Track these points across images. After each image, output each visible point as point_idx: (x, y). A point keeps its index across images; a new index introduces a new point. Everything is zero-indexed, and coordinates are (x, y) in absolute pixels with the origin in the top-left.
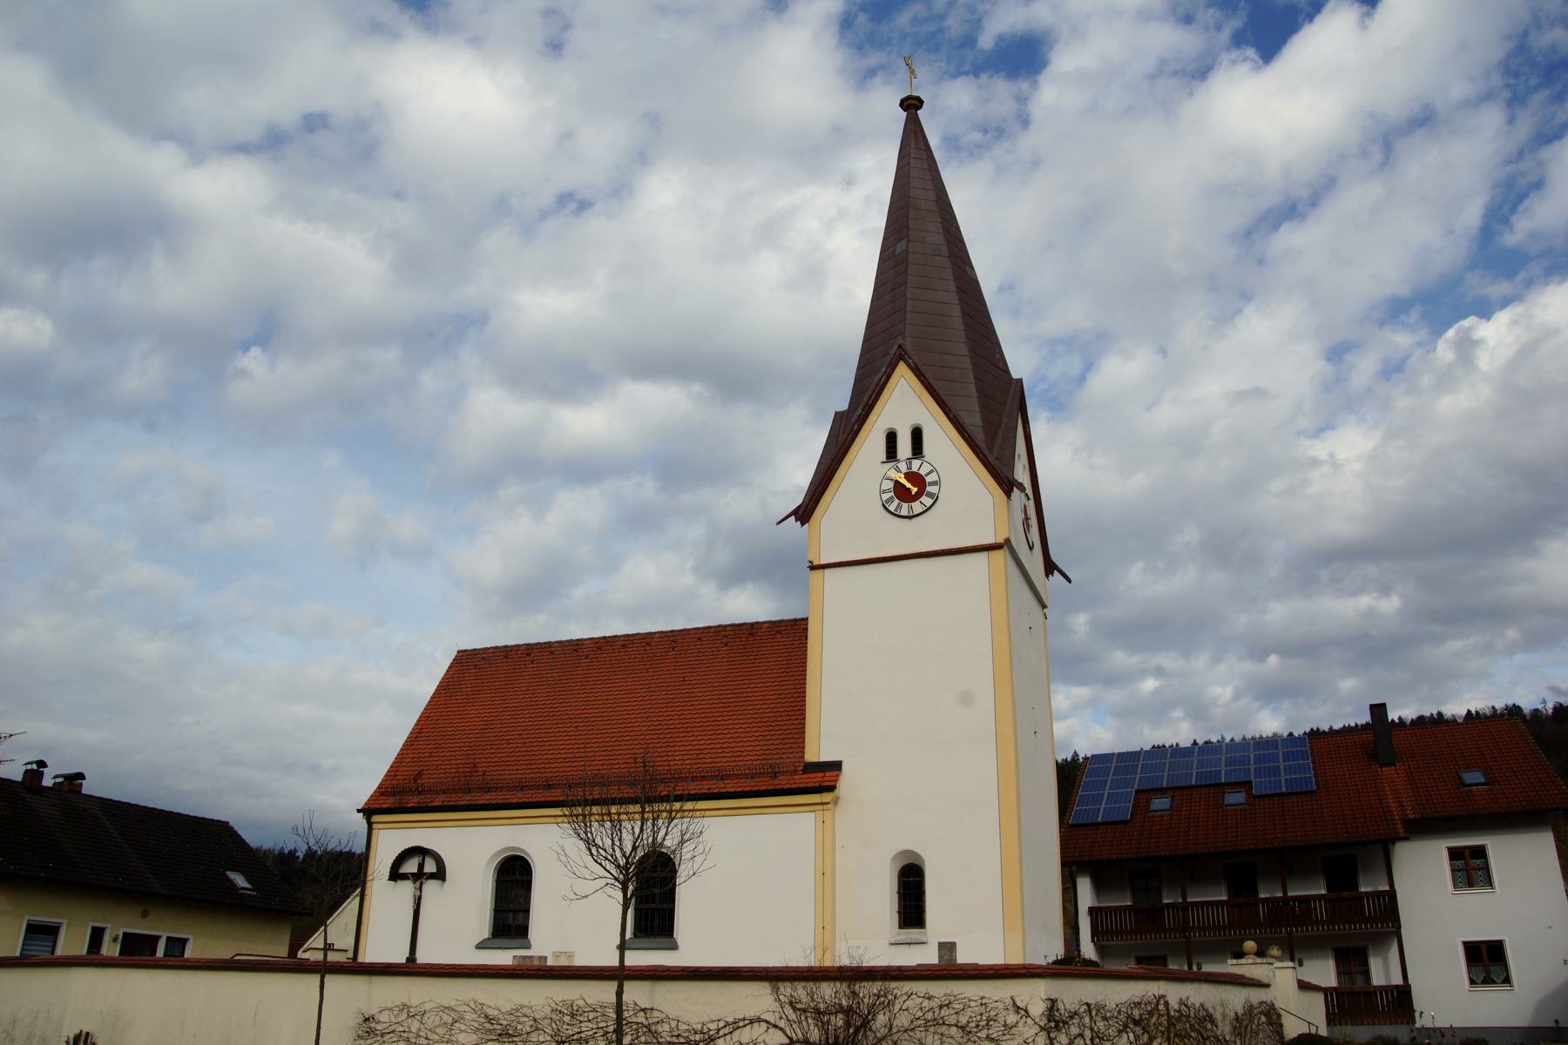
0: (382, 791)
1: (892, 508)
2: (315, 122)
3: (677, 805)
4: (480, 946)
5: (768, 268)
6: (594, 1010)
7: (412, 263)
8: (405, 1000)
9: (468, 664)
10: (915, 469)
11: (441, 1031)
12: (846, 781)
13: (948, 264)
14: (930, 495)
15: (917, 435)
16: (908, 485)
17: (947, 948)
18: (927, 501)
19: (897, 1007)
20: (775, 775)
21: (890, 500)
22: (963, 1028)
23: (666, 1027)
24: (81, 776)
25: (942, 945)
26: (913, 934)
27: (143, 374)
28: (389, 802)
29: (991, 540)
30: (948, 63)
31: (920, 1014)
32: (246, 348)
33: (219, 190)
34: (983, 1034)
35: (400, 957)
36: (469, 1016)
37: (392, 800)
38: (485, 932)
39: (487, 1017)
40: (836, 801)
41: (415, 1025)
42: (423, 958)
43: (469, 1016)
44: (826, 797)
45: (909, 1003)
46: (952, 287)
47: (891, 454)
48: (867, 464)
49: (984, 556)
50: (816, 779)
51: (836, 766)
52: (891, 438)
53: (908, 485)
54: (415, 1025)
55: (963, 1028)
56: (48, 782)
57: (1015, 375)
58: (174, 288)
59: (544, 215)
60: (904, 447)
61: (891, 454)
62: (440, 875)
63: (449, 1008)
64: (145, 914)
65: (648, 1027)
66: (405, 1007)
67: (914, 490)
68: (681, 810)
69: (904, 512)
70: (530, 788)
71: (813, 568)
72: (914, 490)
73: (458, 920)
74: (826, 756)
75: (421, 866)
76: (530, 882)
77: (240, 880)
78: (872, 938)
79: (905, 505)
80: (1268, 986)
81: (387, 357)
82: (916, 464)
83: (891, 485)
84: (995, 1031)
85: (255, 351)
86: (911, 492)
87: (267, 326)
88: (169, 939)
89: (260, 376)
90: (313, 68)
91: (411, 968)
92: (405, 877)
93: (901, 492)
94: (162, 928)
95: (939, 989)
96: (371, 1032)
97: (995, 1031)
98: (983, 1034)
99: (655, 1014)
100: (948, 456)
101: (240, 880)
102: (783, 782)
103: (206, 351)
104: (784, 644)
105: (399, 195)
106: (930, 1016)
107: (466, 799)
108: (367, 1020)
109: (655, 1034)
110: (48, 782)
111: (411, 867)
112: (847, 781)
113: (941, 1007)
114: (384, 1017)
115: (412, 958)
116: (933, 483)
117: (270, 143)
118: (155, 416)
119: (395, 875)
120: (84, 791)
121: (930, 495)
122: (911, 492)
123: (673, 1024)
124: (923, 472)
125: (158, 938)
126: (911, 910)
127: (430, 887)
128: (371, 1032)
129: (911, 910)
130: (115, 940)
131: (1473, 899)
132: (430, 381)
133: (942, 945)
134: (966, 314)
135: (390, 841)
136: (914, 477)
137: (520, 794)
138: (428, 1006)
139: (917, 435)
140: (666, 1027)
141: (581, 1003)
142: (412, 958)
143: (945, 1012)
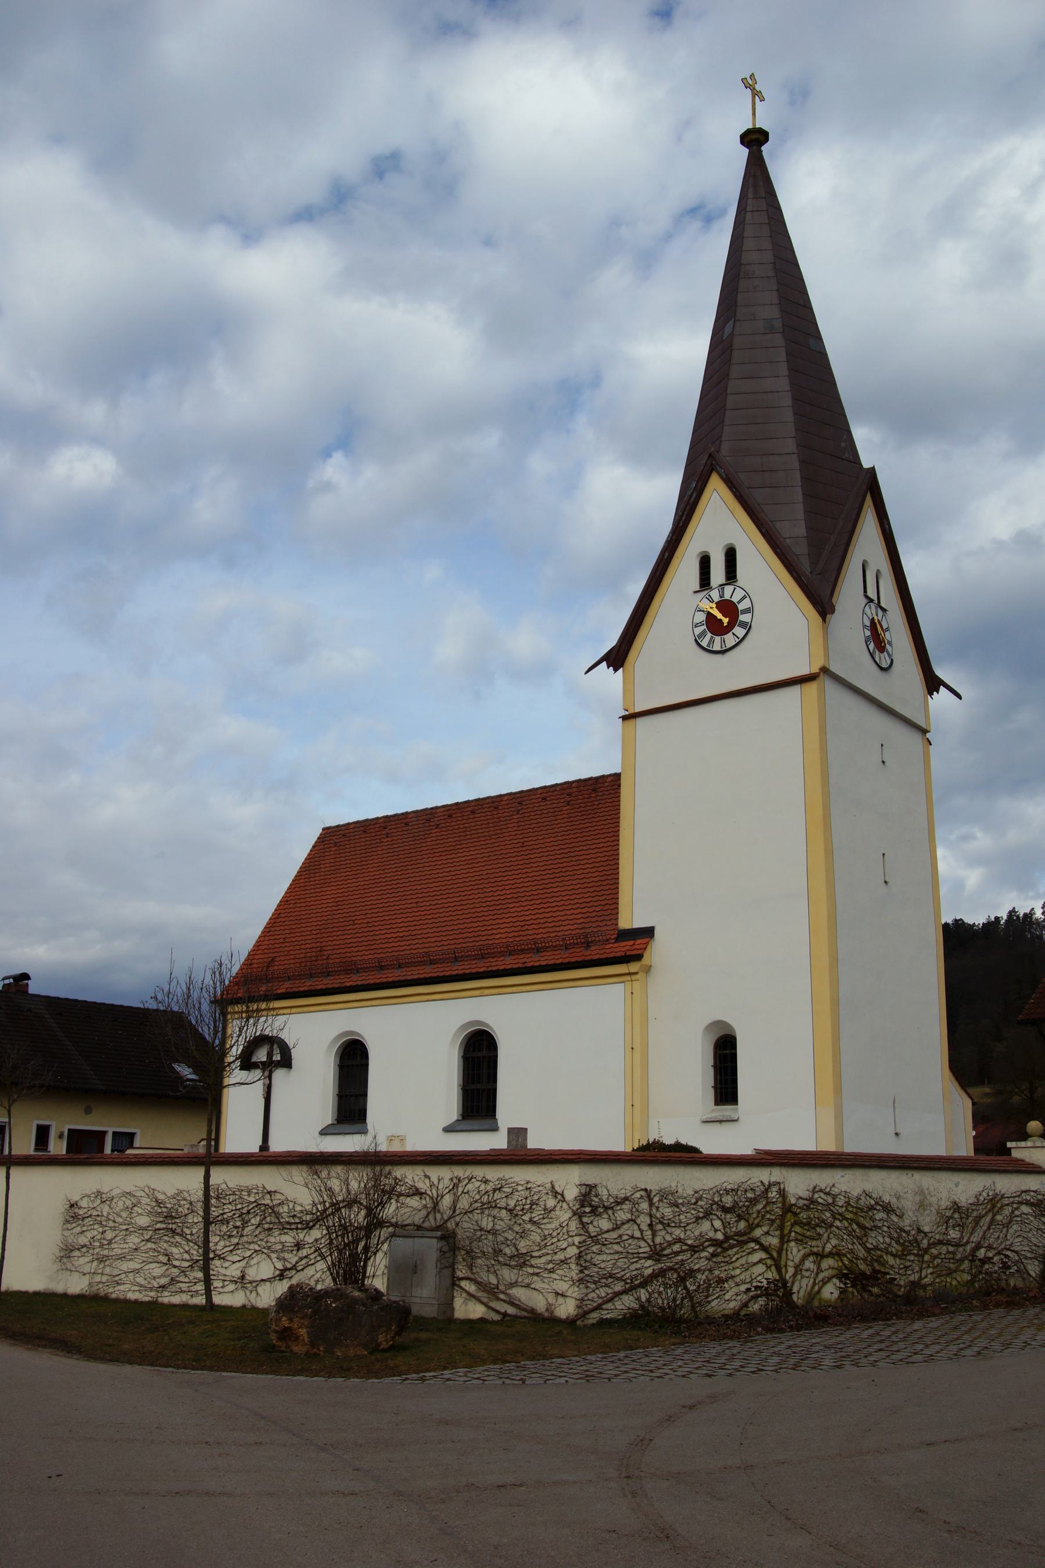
1: (704, 643)
2: (385, 165)
3: (263, 1006)
4: (324, 1133)
5: (951, 263)
6: (234, 1194)
7: (506, 324)
8: (99, 1188)
9: (335, 842)
10: (727, 597)
11: (124, 1214)
13: (778, 340)
14: (743, 625)
15: (731, 555)
16: (719, 616)
17: (518, 1134)
18: (739, 631)
19: (460, 1189)
20: (588, 945)
21: (702, 635)
22: (511, 1211)
23: (286, 1208)
25: (511, 1131)
26: (726, 1110)
27: (214, 502)
29: (804, 671)
31: (477, 1197)
32: (327, 454)
33: (281, 272)
34: (526, 1218)
36: (145, 1200)
38: (328, 1116)
39: (157, 1201)
40: (648, 969)
41: (106, 1209)
43: (145, 1200)
44: (634, 967)
45: (470, 1187)
46: (783, 369)
48: (682, 602)
49: (796, 690)
51: (648, 933)
52: (705, 562)
53: (719, 616)
54: (106, 1209)
55: (511, 1211)
57: (866, 464)
58: (256, 389)
59: (668, 237)
62: (286, 1062)
63: (129, 1193)
64: (88, 1111)
65: (272, 1208)
66: (99, 1193)
67: (726, 621)
68: (269, 1009)
69: (717, 647)
70: (408, 965)
72: (726, 621)
73: (301, 1108)
74: (638, 923)
75: (270, 1055)
76: (367, 1065)
77: (185, 1071)
78: (681, 1112)
79: (718, 639)
81: (489, 442)
82: (728, 590)
83: (701, 617)
84: (537, 1214)
85: (338, 457)
86: (724, 622)
87: (348, 425)
88: (114, 1133)
89: (347, 486)
90: (373, 97)
91: (264, 1158)
93: (714, 626)
94: (107, 1122)
95: (493, 1173)
96: (75, 1217)
97: (537, 1214)
98: (526, 1218)
99: (278, 1196)
101: (185, 1071)
102: (594, 953)
103: (281, 461)
105: (488, 242)
106: (485, 1199)
107: (308, 985)
108: (72, 1206)
109: (278, 1215)
111: (261, 1055)
112: (658, 951)
113: (494, 1190)
114: (84, 1203)
115: (265, 1146)
116: (746, 611)
117: (332, 206)
118: (234, 550)
119: (247, 1063)
121: (743, 625)
122: (724, 622)
123: (291, 1205)
124: (735, 599)
125: (104, 1133)
126: (726, 1088)
127: (279, 1074)
128: (75, 1217)
129: (726, 1088)
130: (61, 1136)
132: (540, 465)
133: (511, 1131)
134: (800, 400)
136: (728, 607)
137: (398, 972)
138: (115, 1193)
139: (731, 555)
140: (286, 1208)
141: (224, 1186)
143: (497, 1195)
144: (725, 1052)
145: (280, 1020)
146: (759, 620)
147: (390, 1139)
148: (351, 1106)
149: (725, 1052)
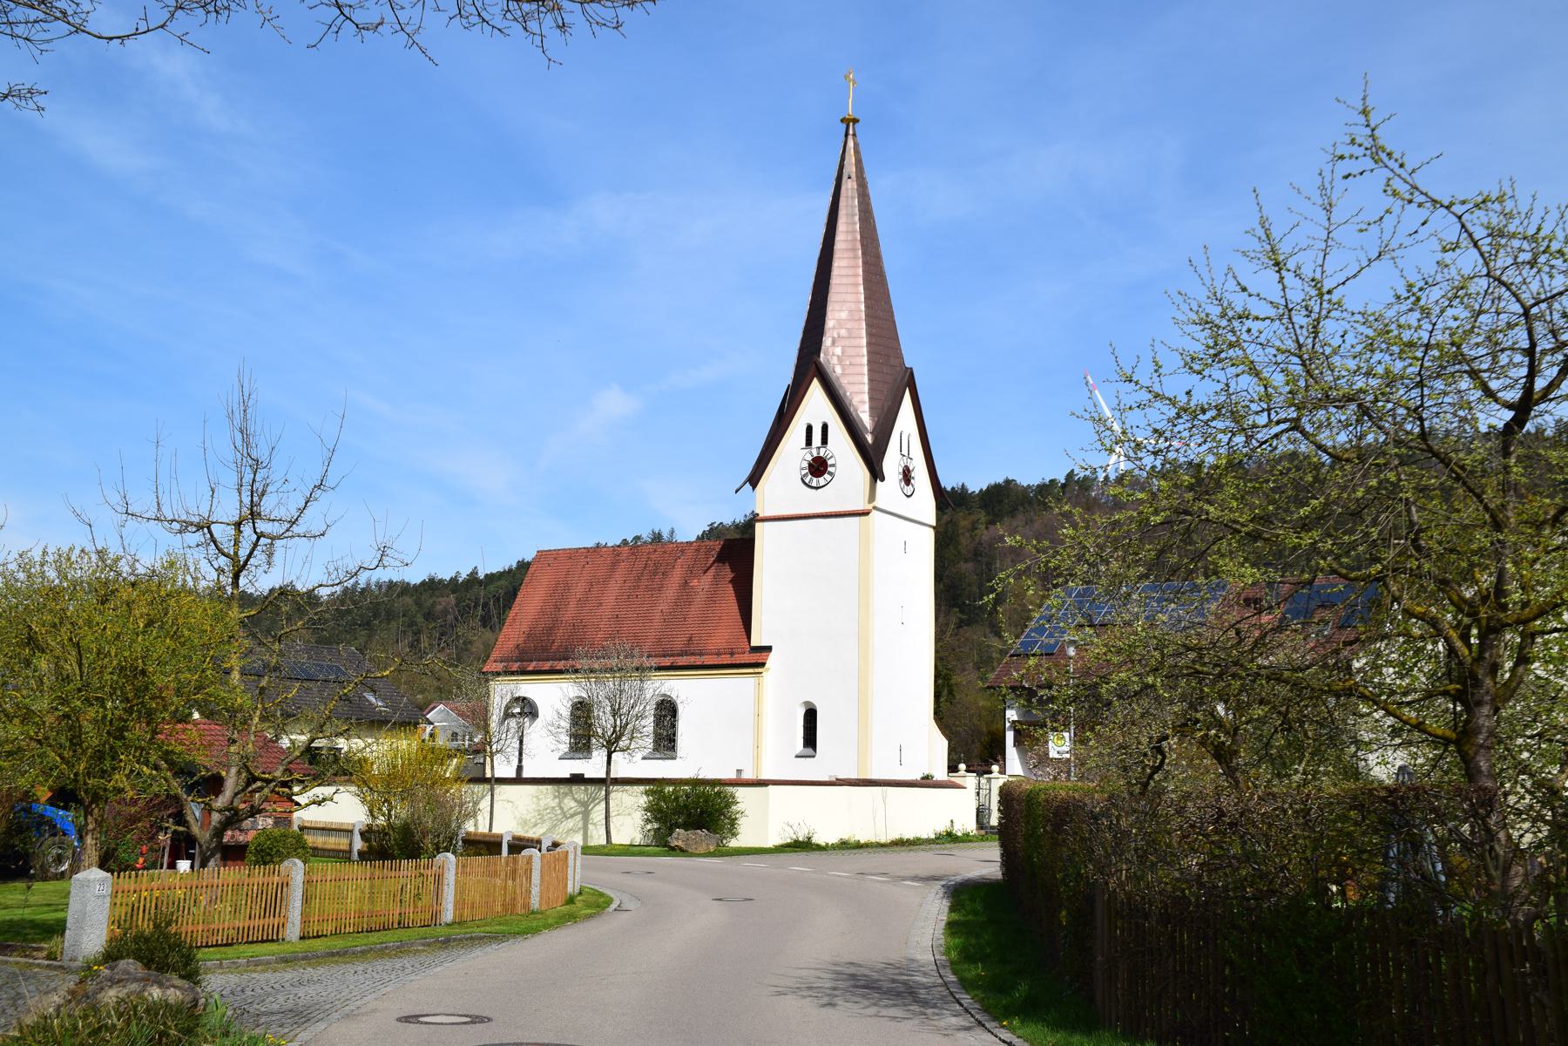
12: (772, 660)
14: (831, 474)
15: (825, 428)
20: (732, 654)
30: (1382, 335)
35: (513, 775)
37: (307, 994)
38: (565, 748)
42: (525, 774)
47: (809, 442)
50: (754, 658)
51: (769, 649)
52: (809, 429)
61: (809, 442)
82: (822, 451)
86: (818, 467)
92: (513, 715)
100: (841, 449)
122: (818, 467)
126: (810, 739)
129: (810, 739)
139: (825, 428)
144: (811, 716)
148: (666, 742)
149: (811, 716)
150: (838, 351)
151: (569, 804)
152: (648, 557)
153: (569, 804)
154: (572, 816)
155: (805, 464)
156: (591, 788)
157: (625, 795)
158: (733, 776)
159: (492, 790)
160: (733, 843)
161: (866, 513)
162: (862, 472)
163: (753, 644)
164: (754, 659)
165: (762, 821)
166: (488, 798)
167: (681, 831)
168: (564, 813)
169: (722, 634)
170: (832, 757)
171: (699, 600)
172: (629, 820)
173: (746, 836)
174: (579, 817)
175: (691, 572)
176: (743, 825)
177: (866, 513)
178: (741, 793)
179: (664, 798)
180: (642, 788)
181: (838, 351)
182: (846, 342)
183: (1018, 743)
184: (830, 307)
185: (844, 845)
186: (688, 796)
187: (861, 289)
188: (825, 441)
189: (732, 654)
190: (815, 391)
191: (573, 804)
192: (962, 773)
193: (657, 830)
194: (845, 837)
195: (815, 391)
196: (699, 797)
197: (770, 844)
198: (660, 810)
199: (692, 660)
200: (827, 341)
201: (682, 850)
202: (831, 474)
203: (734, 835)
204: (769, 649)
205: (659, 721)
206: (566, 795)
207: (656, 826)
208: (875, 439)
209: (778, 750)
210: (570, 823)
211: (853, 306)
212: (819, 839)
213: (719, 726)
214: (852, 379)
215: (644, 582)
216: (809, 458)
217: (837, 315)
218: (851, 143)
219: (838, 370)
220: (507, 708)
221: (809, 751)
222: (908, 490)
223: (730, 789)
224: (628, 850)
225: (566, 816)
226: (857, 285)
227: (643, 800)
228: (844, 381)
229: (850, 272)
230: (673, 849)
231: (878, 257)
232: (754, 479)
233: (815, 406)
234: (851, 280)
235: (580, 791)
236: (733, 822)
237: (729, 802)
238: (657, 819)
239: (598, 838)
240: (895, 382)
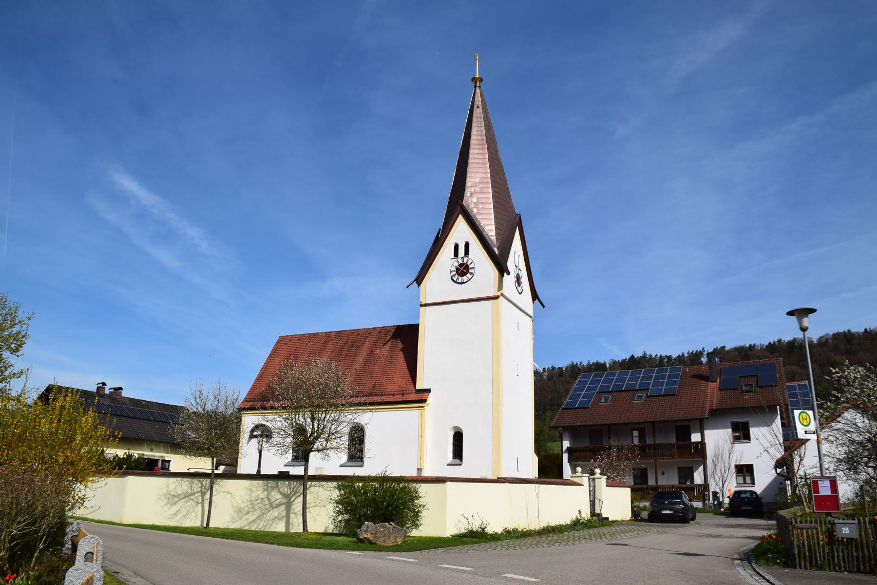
0: (246, 400)
12: (431, 398)
14: (471, 273)
15: (467, 245)
18: (469, 276)
20: (403, 394)
21: (454, 275)
24: (121, 389)
28: (249, 405)
48: (445, 260)
51: (429, 391)
52: (456, 247)
56: (107, 392)
60: (462, 252)
69: (460, 281)
71: (422, 305)
80: (341, 466)
82: (465, 260)
86: (463, 270)
92: (256, 436)
100: (479, 257)
104: (407, 337)
110: (107, 392)
115: (259, 471)
116: (473, 268)
119: (252, 436)
120: (123, 395)
121: (471, 273)
122: (463, 270)
126: (458, 452)
129: (458, 452)
131: (740, 447)
135: (249, 421)
139: (467, 245)
142: (259, 471)
144: (458, 437)
145: (368, 415)
146: (477, 272)
147: (317, 468)
148: (356, 455)
149: (458, 437)
150: (475, 200)
151: (276, 496)
152: (346, 343)
153: (276, 496)
154: (278, 506)
155: (454, 269)
156: (294, 484)
157: (321, 489)
158: (414, 474)
159: (305, 489)
160: (415, 533)
161: (496, 298)
162: (493, 271)
163: (417, 388)
164: (420, 398)
165: (443, 513)
166: (209, 493)
167: (370, 524)
168: (270, 503)
169: (397, 381)
170: (469, 467)
171: (380, 362)
172: (322, 512)
173: (430, 526)
174: (283, 508)
175: (375, 345)
176: (425, 517)
177: (496, 298)
178: (423, 489)
179: (355, 492)
180: (335, 484)
181: (475, 200)
182: (480, 196)
183: (569, 461)
184: (468, 175)
185: (511, 535)
186: (375, 490)
187: (488, 165)
188: (467, 252)
189: (403, 394)
190: (461, 223)
191: (278, 496)
192: (579, 474)
193: (348, 520)
194: (510, 527)
195: (461, 223)
196: (386, 491)
197: (447, 534)
198: (350, 503)
199: (375, 399)
200: (467, 194)
201: (370, 542)
202: (472, 274)
203: (417, 526)
204: (429, 391)
205: (351, 439)
206: (273, 488)
207: (346, 517)
208: (500, 251)
209: (437, 462)
210: (275, 512)
211: (483, 175)
212: (490, 530)
213: (394, 442)
214: (484, 217)
215: (345, 352)
216: (457, 264)
217: (473, 180)
218: (478, 91)
219: (475, 211)
220: (252, 431)
221: (457, 461)
222: (520, 289)
223: (414, 485)
224: (321, 541)
225: (273, 506)
226: (485, 163)
227: (336, 494)
228: (479, 217)
229: (481, 161)
230: (362, 541)
231: (496, 151)
232: (419, 280)
233: (461, 231)
234: (481, 161)
235: (284, 486)
236: (416, 515)
237: (413, 496)
238: (347, 511)
239: (297, 527)
240: (510, 222)
